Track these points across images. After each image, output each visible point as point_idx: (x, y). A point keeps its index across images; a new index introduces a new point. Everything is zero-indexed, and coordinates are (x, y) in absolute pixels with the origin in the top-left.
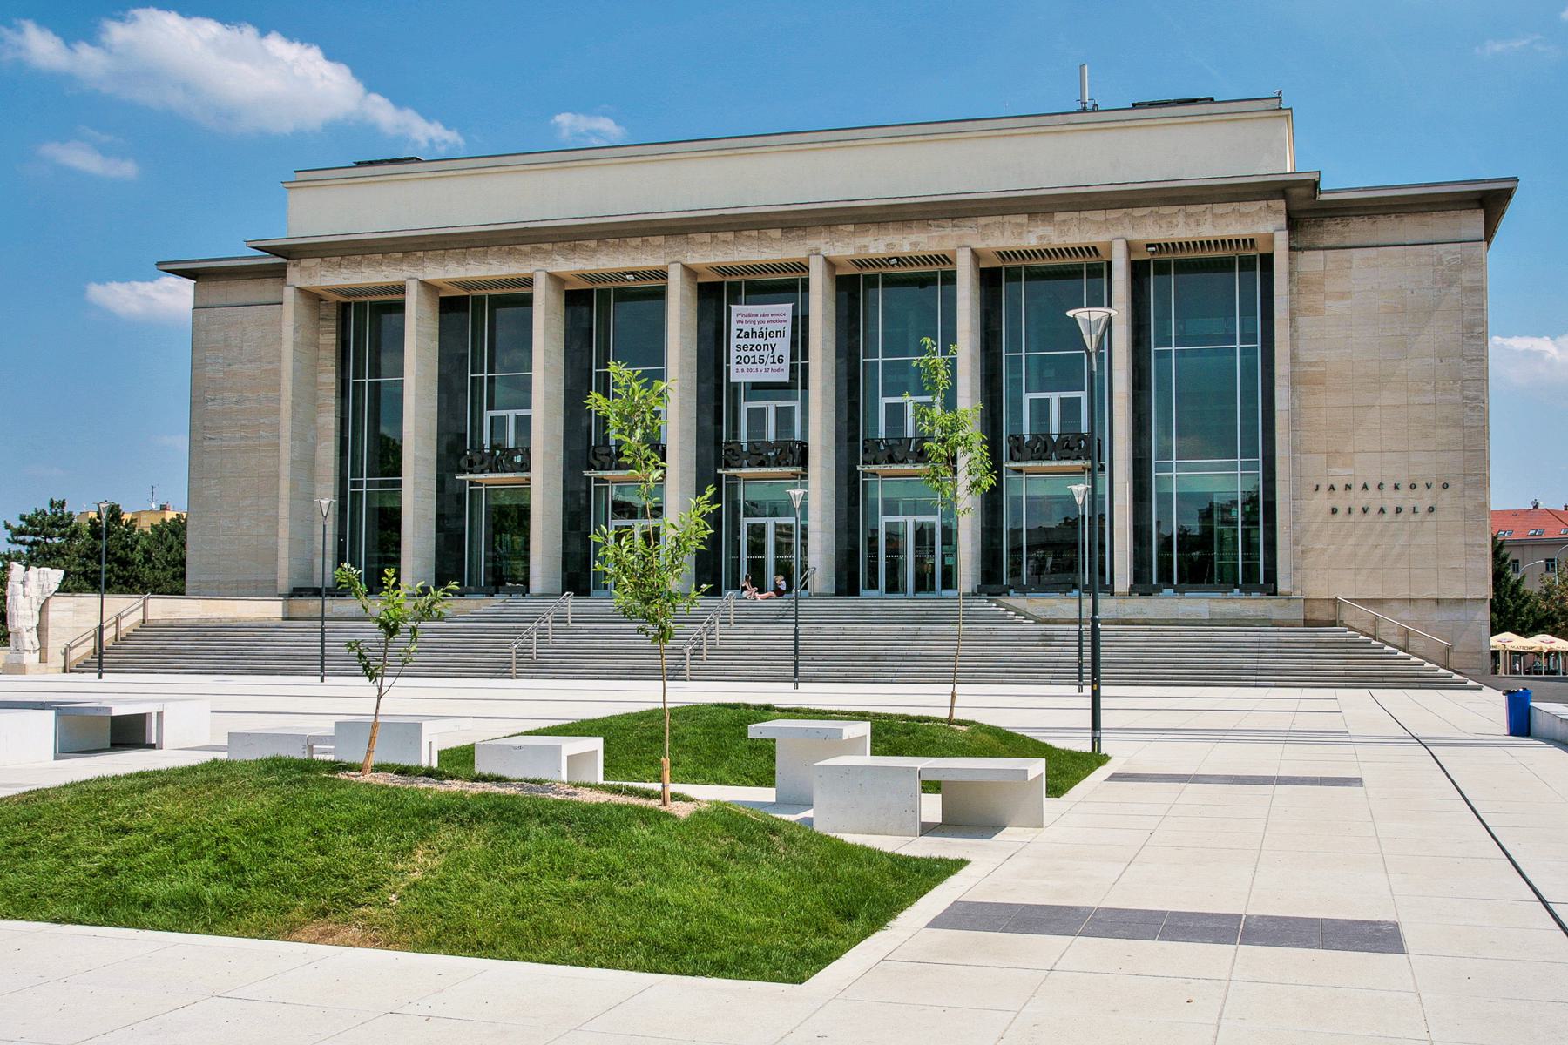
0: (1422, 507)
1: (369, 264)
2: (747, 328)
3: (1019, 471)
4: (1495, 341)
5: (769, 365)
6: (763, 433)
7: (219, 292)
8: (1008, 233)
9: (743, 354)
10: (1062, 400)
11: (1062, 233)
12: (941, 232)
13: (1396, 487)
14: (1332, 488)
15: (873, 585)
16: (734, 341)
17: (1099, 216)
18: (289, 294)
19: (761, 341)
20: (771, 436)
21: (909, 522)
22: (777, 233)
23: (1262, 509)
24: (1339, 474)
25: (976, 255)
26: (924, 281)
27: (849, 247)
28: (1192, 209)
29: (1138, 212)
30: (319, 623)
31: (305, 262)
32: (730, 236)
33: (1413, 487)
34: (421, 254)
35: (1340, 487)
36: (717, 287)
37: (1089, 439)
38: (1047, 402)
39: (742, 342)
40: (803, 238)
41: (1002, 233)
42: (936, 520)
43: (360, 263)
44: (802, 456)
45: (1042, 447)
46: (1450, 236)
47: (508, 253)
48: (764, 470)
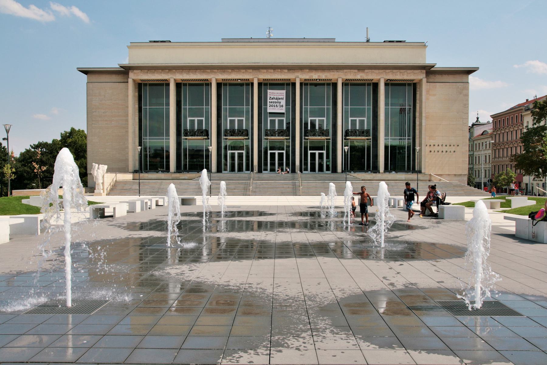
0: (452, 151)
2: (272, 97)
3: (186, 139)
6: (275, 127)
7: (95, 78)
8: (352, 74)
9: (271, 104)
10: (198, 120)
15: (226, 170)
16: (269, 100)
17: (377, 71)
18: (130, 81)
19: (277, 101)
20: (277, 128)
22: (286, 71)
23: (412, 149)
24: (432, 142)
25: (216, 80)
26: (162, 85)
27: (222, 76)
28: (402, 71)
29: (387, 71)
31: (135, 71)
32: (272, 71)
33: (450, 146)
35: (432, 145)
37: (247, 131)
39: (271, 101)
40: (294, 72)
43: (154, 73)
46: (461, 81)
47: (203, 72)
48: (193, 137)
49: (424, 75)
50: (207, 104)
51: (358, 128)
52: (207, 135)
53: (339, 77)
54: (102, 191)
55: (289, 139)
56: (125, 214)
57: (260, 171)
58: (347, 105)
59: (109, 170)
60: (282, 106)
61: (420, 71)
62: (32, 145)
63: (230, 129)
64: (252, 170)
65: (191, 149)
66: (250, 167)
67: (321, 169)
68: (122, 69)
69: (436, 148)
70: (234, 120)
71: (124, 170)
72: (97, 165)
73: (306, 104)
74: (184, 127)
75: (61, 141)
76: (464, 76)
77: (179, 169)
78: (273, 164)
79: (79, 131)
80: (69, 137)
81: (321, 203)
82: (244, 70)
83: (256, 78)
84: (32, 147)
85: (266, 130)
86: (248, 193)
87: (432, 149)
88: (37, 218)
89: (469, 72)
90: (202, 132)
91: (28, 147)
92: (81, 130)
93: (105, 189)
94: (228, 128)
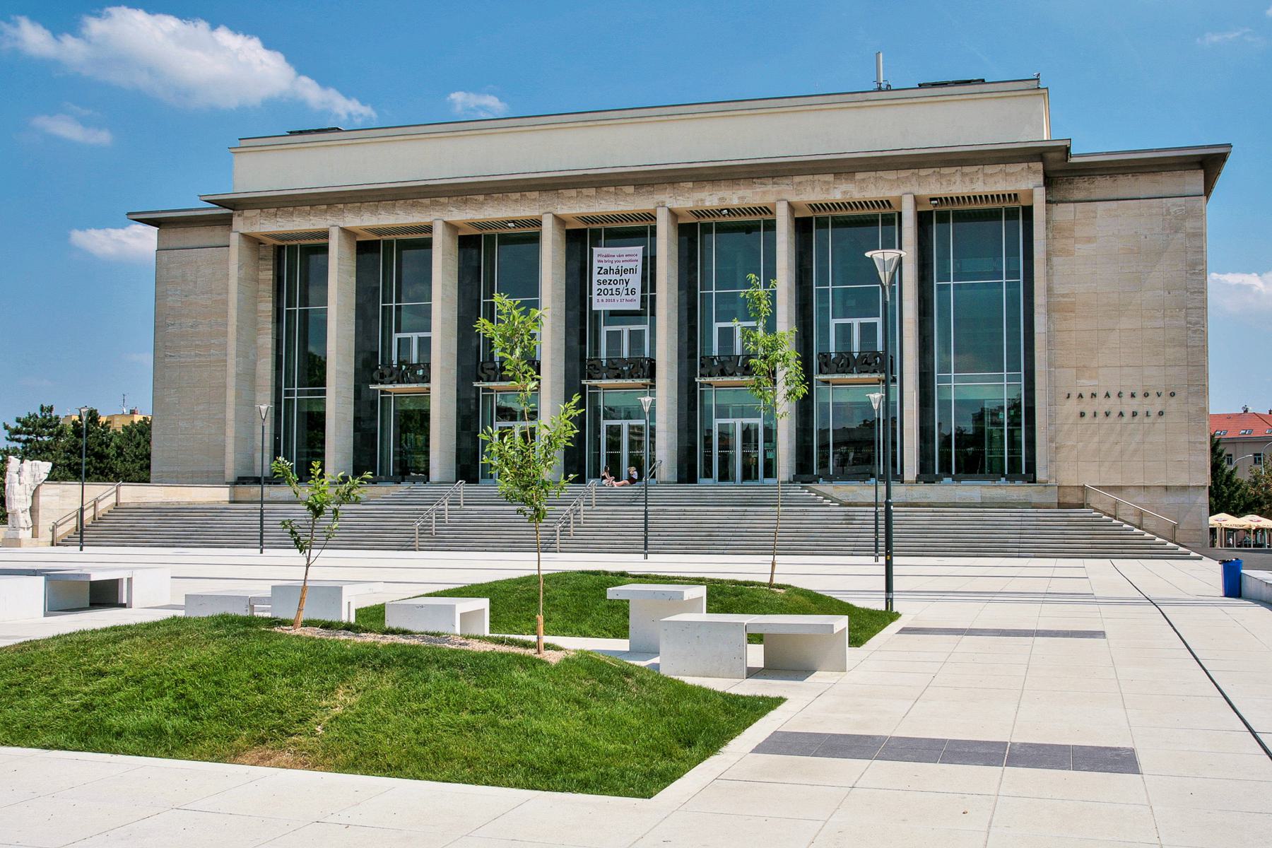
0: (1154, 411)
1: (300, 215)
2: (606, 266)
3: (827, 382)
4: (1212, 277)
5: (624, 296)
6: (619, 352)
7: (178, 237)
8: (817, 189)
9: (602, 287)
10: (862, 325)
11: (862, 189)
12: (763, 189)
13: (1133, 395)
14: (1081, 396)
15: (708, 475)
16: (596, 277)
17: (892, 175)
18: (234, 239)
19: (618, 277)
20: (626, 354)
21: (737, 424)
22: (630, 189)
23: (1023, 413)
24: (1086, 385)
25: (792, 207)
26: (750, 228)
27: (689, 200)
28: (967, 169)
29: (923, 172)
30: (259, 506)
31: (247, 213)
32: (592, 191)
33: (1146, 395)
34: (341, 206)
35: (1087, 395)
36: (582, 233)
37: (884, 356)
38: (849, 326)
39: (602, 277)
40: (651, 193)
41: (813, 189)
42: (759, 422)
43: (292, 214)
44: (650, 370)
45: (845, 363)
46: (1177, 191)
47: (412, 206)
48: (620, 381)
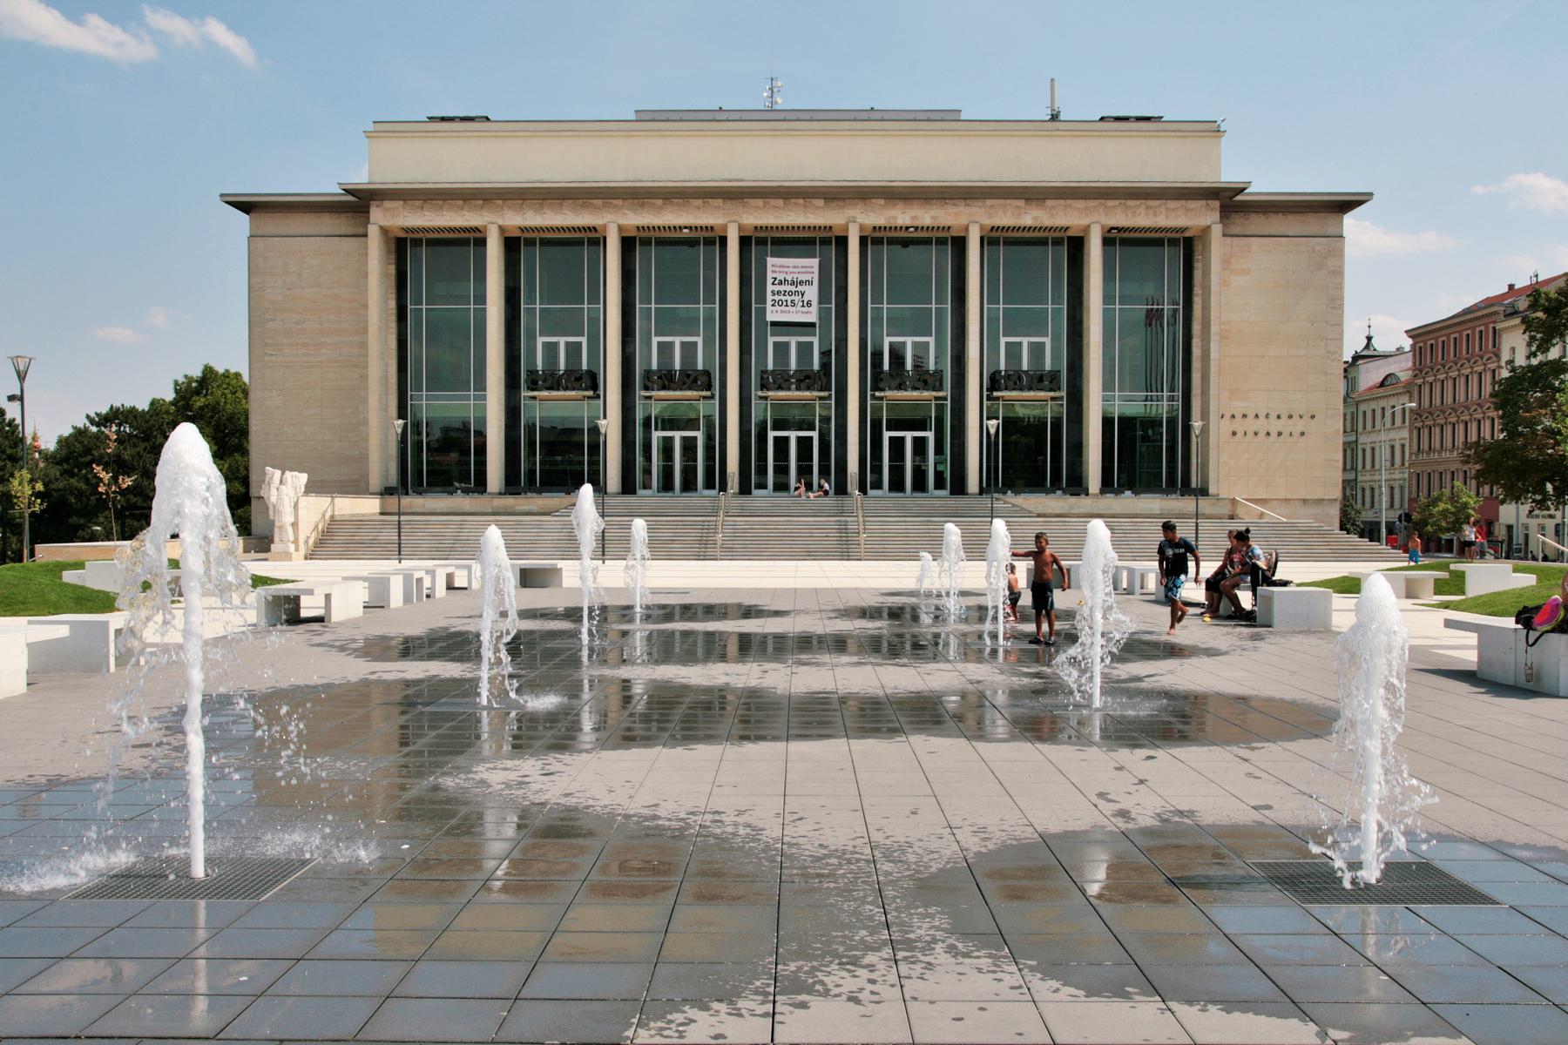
0: (1296, 432)
2: (780, 277)
3: (534, 398)
6: (788, 363)
7: (271, 223)
8: (1009, 213)
9: (777, 298)
10: (567, 344)
15: (646, 486)
16: (770, 288)
17: (1080, 204)
18: (373, 231)
19: (793, 288)
20: (793, 366)
22: (821, 203)
23: (1180, 427)
24: (1238, 407)
25: (620, 228)
26: (464, 243)
27: (636, 219)
28: (1151, 203)
29: (1111, 203)
31: (387, 204)
32: (780, 202)
33: (1290, 417)
35: (1238, 416)
37: (707, 374)
39: (777, 288)
40: (842, 207)
43: (441, 208)
46: (1321, 232)
47: (582, 206)
48: (554, 393)
49: (1216, 216)
50: (594, 298)
51: (1025, 367)
52: (595, 387)
53: (973, 221)
54: (292, 548)
55: (829, 397)
56: (360, 612)
57: (745, 489)
58: (993, 299)
59: (313, 488)
60: (809, 304)
61: (1203, 202)
62: (92, 415)
63: (659, 370)
64: (723, 488)
65: (547, 426)
66: (716, 480)
67: (920, 485)
68: (350, 198)
69: (1251, 425)
70: (672, 344)
71: (356, 487)
72: (278, 473)
73: (877, 299)
74: (527, 364)
75: (174, 403)
76: (1331, 219)
77: (513, 484)
78: (782, 470)
79: (227, 375)
80: (197, 392)
81: (920, 580)
82: (700, 201)
83: (733, 222)
84: (92, 422)
85: (764, 373)
86: (710, 551)
87: (1239, 425)
88: (106, 624)
89: (1345, 205)
90: (579, 379)
91: (81, 422)
92: (232, 371)
93: (301, 542)
94: (655, 367)
